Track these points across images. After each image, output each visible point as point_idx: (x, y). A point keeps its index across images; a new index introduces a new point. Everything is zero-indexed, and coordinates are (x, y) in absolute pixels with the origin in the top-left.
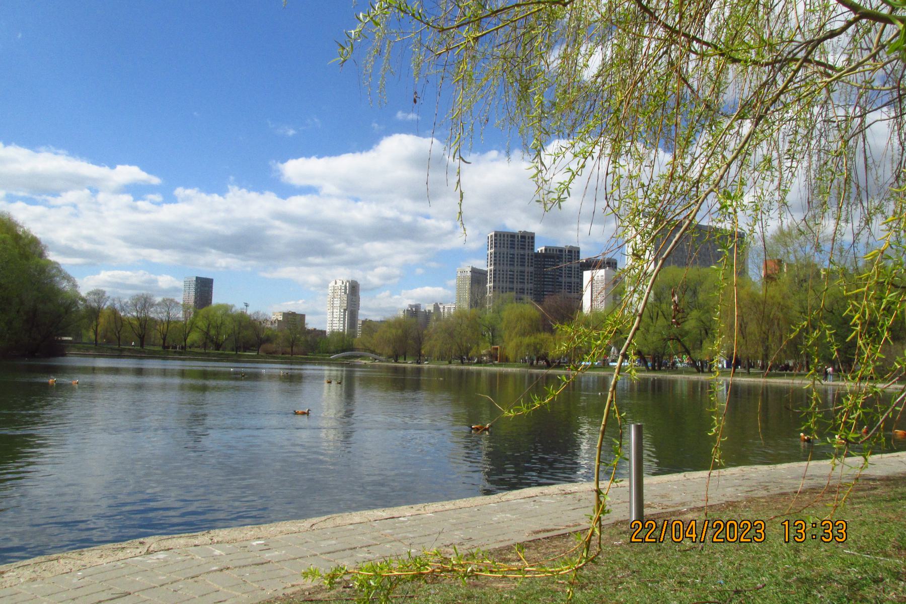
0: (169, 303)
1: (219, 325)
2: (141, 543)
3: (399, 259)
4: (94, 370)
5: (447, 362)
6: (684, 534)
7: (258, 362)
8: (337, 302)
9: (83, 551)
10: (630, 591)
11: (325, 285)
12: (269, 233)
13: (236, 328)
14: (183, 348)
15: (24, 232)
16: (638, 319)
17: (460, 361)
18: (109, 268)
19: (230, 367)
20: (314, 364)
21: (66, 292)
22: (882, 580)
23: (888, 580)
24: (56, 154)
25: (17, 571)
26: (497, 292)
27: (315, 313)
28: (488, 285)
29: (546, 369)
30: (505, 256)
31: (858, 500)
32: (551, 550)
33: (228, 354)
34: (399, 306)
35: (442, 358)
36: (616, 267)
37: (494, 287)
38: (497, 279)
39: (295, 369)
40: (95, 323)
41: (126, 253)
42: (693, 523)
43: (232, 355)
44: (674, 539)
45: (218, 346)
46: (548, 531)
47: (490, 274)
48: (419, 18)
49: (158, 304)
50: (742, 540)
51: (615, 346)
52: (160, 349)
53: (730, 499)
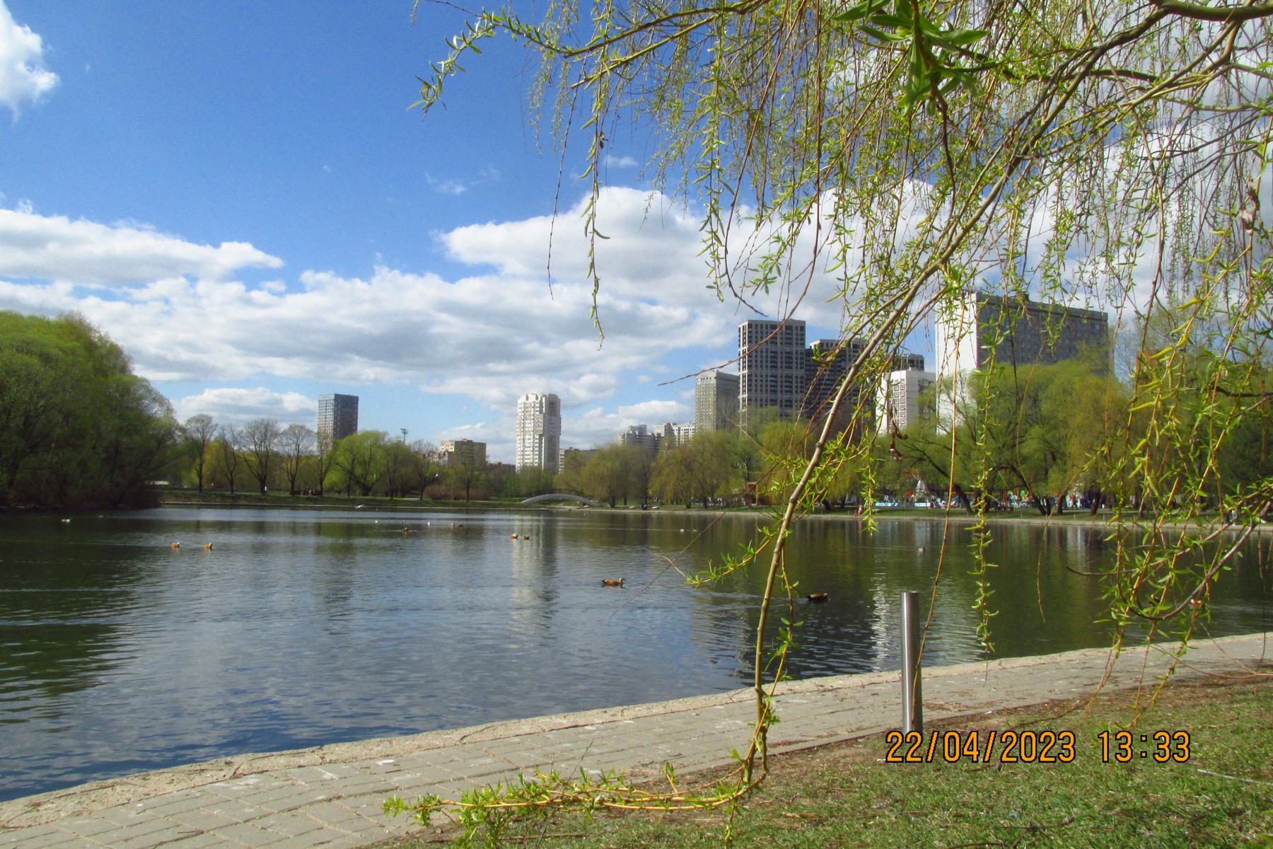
0: (298, 432)
1: (367, 459)
2: (227, 763)
3: (614, 363)
4: (198, 526)
5: (684, 506)
6: (961, 750)
7: (421, 511)
8: (530, 425)
9: (148, 775)
10: (884, 829)
11: (512, 402)
12: (435, 330)
13: (391, 464)
14: (320, 493)
15: (101, 338)
16: (817, 451)
17: (702, 505)
18: (217, 385)
19: (376, 518)
20: (501, 512)
21: (158, 420)
22: (1240, 812)
23: (1249, 812)
24: (139, 230)
25: (58, 802)
26: (753, 407)
27: (499, 441)
28: (741, 397)
29: (824, 512)
30: (764, 355)
31: (1242, 697)
32: (788, 770)
33: (380, 501)
34: (616, 429)
35: (676, 500)
36: (922, 368)
37: (749, 400)
38: (754, 388)
39: (472, 520)
40: (198, 461)
41: (240, 364)
42: (974, 735)
43: (386, 501)
44: (947, 757)
45: (366, 490)
46: (790, 743)
47: (744, 381)
48: (537, 39)
49: (283, 434)
50: (1043, 758)
51: (922, 479)
52: (287, 494)
53: (1061, 697)
